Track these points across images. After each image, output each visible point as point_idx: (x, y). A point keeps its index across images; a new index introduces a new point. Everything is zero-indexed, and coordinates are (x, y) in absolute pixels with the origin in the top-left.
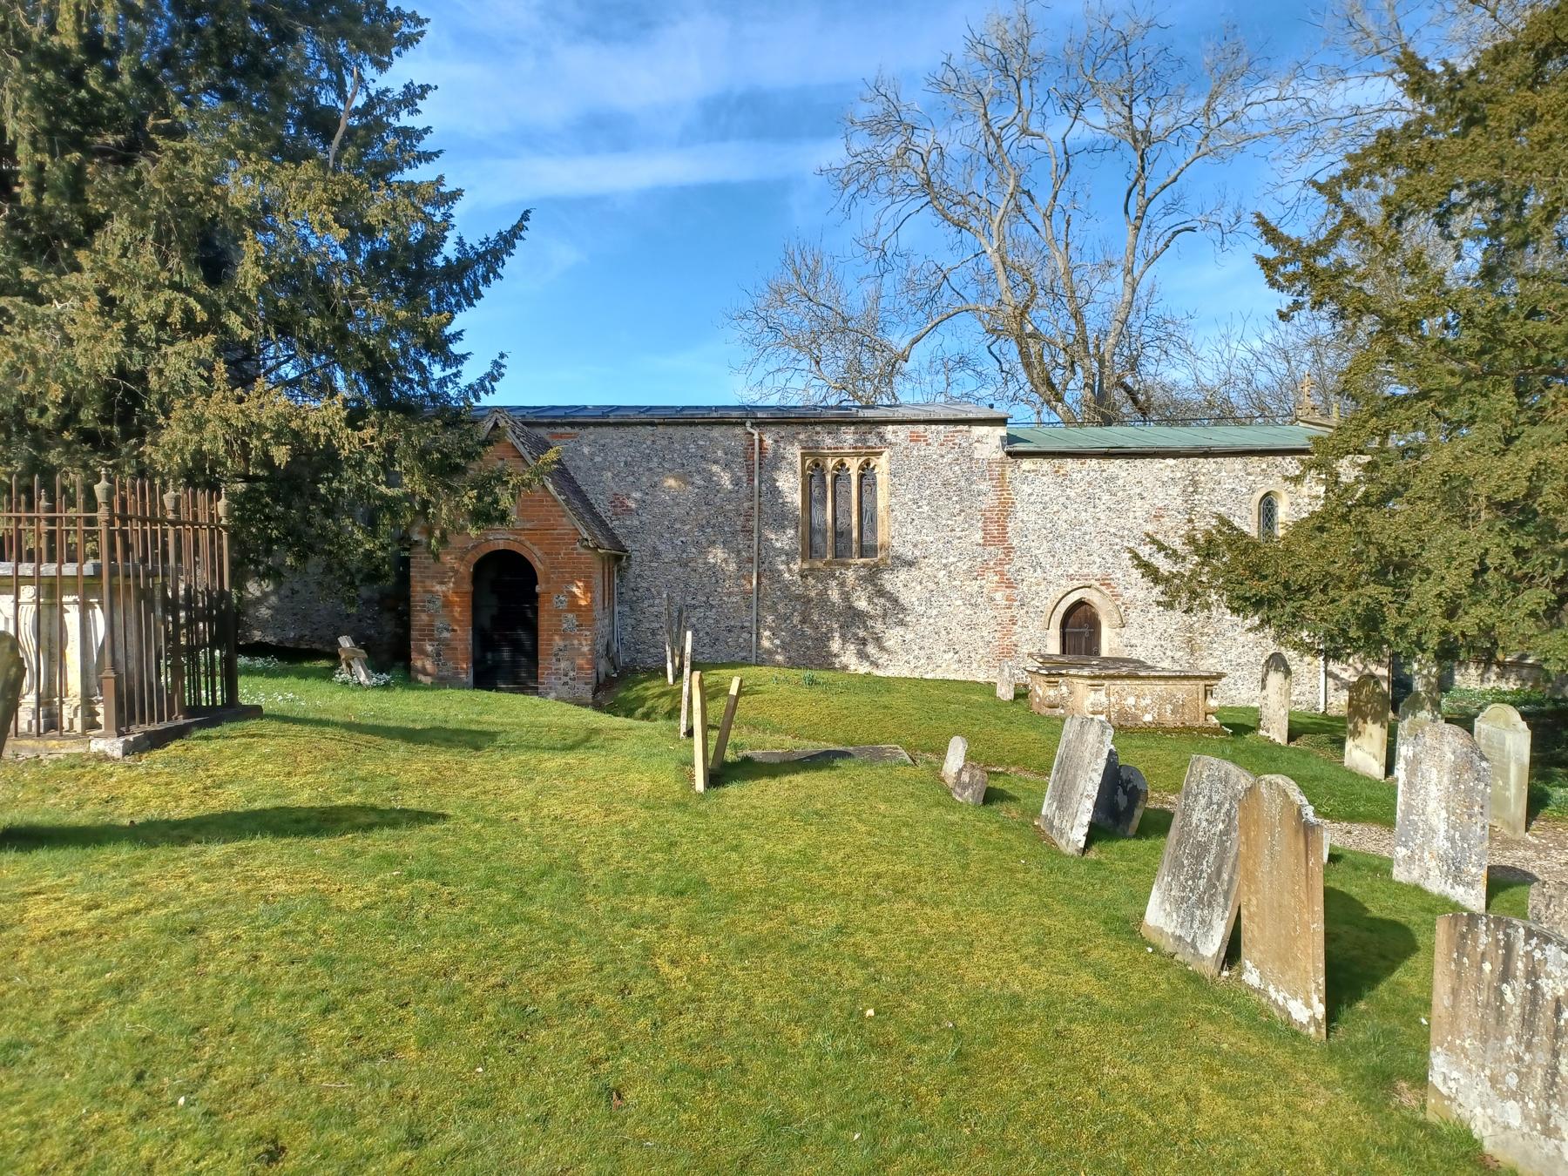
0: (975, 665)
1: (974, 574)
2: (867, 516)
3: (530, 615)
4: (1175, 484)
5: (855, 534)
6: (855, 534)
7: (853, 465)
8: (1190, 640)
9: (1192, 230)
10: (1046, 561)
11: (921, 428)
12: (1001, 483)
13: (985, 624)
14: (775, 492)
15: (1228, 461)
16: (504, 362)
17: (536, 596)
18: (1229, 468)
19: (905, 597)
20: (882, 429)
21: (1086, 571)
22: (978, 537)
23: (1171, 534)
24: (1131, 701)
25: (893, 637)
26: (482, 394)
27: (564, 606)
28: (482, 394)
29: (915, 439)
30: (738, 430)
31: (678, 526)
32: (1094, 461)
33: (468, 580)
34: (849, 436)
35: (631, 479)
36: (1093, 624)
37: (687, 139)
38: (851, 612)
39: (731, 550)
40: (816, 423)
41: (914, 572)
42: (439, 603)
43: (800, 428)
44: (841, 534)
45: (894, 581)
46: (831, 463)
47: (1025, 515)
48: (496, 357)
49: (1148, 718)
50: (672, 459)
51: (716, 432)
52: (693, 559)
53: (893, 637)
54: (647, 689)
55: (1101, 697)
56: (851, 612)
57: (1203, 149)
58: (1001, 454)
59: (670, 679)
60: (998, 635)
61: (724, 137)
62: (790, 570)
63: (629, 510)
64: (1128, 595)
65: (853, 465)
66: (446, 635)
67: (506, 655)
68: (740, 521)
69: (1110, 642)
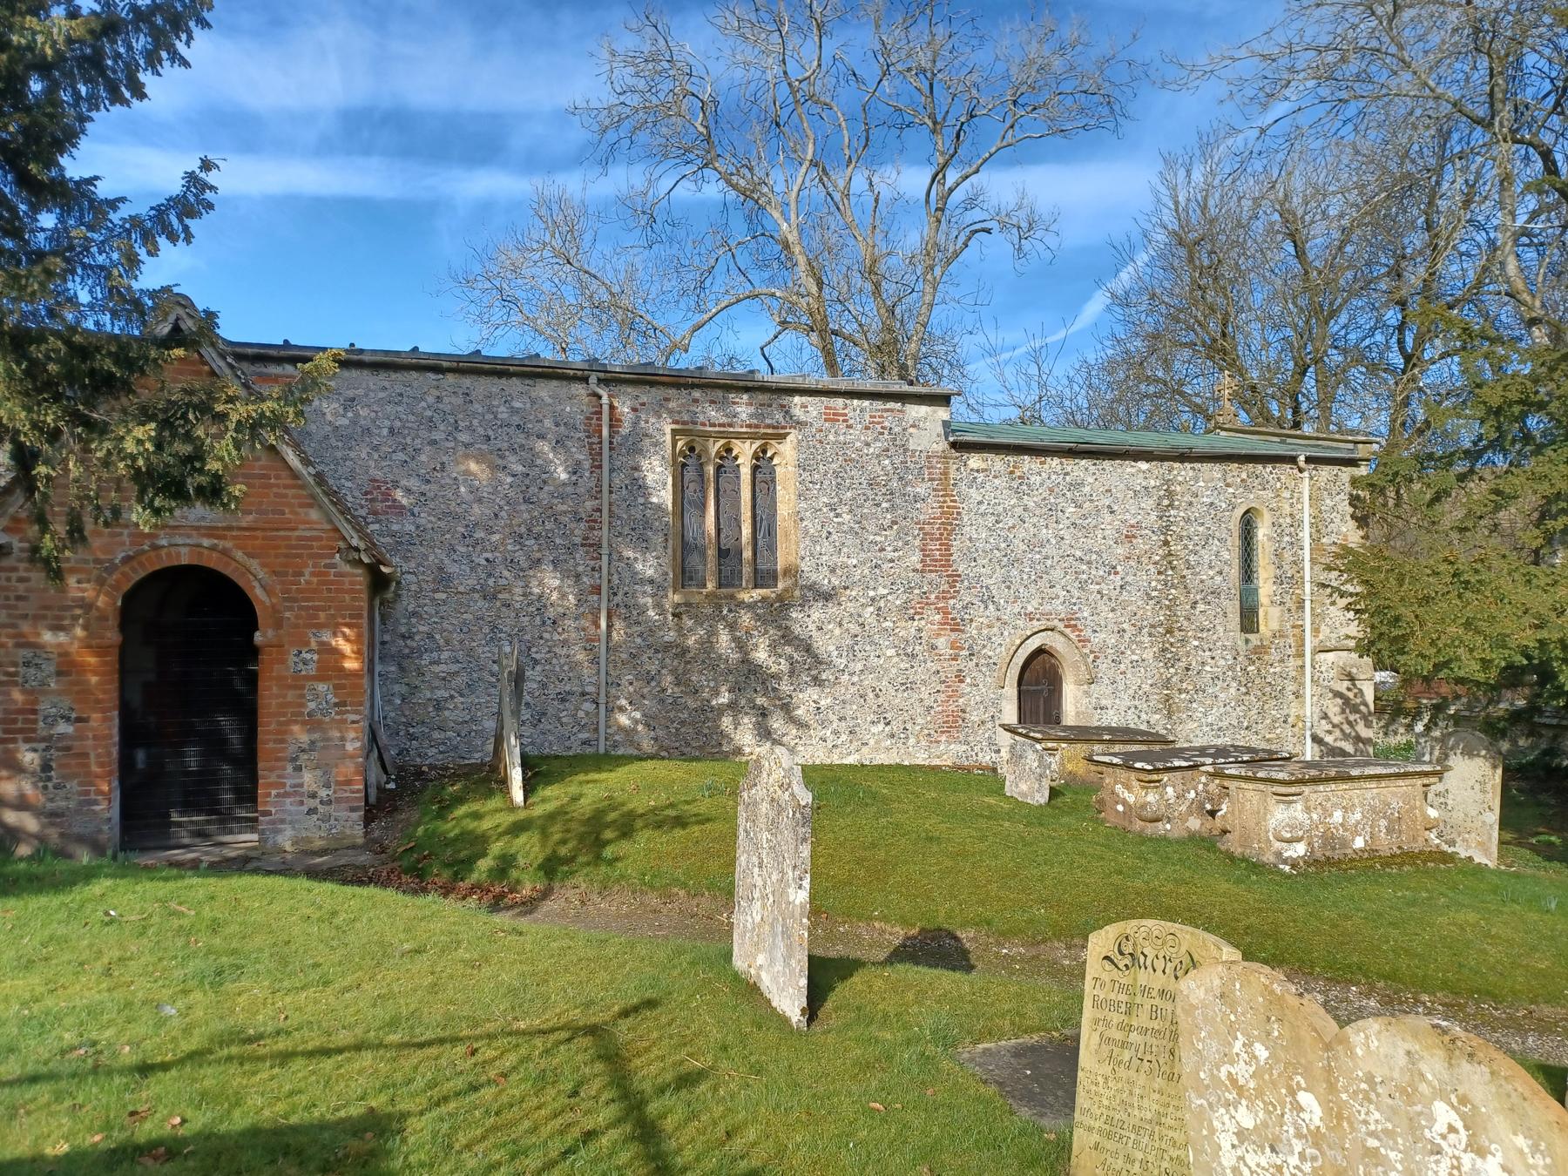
0: (912, 741)
1: (909, 613)
2: (764, 524)
3: (239, 685)
4: (1148, 494)
5: (747, 554)
6: (747, 554)
7: (745, 452)
8: (1168, 698)
9: (988, 231)
10: (1001, 595)
11: (840, 402)
12: (944, 485)
13: (924, 682)
14: (638, 487)
15: (1206, 467)
16: (211, 178)
17: (253, 652)
18: (1207, 476)
19: (825, 645)
20: (786, 400)
21: (1047, 608)
22: (915, 559)
23: (1144, 560)
24: (1338, 816)
25: (806, 700)
26: (162, 241)
27: (312, 669)
28: (162, 241)
29: (833, 417)
30: (579, 389)
31: (480, 534)
32: (1056, 461)
33: (113, 622)
34: (743, 408)
35: (401, 456)
36: (1052, 681)
37: (323, 149)
38: (745, 668)
39: (565, 575)
40: (694, 386)
41: (832, 609)
42: (50, 668)
43: (672, 392)
44: (728, 555)
45: (809, 621)
46: (715, 447)
47: (974, 530)
48: (194, 165)
49: (1359, 843)
50: (470, 428)
51: (544, 391)
52: (505, 589)
53: (806, 700)
54: (477, 816)
55: (1297, 811)
56: (745, 668)
57: (1009, 138)
58: (943, 445)
59: (518, 795)
60: (942, 697)
61: (367, 151)
62: (658, 605)
63: (399, 509)
64: (1097, 640)
65: (745, 452)
66: (63, 728)
67: (192, 760)
68: (579, 530)
69: (1074, 704)
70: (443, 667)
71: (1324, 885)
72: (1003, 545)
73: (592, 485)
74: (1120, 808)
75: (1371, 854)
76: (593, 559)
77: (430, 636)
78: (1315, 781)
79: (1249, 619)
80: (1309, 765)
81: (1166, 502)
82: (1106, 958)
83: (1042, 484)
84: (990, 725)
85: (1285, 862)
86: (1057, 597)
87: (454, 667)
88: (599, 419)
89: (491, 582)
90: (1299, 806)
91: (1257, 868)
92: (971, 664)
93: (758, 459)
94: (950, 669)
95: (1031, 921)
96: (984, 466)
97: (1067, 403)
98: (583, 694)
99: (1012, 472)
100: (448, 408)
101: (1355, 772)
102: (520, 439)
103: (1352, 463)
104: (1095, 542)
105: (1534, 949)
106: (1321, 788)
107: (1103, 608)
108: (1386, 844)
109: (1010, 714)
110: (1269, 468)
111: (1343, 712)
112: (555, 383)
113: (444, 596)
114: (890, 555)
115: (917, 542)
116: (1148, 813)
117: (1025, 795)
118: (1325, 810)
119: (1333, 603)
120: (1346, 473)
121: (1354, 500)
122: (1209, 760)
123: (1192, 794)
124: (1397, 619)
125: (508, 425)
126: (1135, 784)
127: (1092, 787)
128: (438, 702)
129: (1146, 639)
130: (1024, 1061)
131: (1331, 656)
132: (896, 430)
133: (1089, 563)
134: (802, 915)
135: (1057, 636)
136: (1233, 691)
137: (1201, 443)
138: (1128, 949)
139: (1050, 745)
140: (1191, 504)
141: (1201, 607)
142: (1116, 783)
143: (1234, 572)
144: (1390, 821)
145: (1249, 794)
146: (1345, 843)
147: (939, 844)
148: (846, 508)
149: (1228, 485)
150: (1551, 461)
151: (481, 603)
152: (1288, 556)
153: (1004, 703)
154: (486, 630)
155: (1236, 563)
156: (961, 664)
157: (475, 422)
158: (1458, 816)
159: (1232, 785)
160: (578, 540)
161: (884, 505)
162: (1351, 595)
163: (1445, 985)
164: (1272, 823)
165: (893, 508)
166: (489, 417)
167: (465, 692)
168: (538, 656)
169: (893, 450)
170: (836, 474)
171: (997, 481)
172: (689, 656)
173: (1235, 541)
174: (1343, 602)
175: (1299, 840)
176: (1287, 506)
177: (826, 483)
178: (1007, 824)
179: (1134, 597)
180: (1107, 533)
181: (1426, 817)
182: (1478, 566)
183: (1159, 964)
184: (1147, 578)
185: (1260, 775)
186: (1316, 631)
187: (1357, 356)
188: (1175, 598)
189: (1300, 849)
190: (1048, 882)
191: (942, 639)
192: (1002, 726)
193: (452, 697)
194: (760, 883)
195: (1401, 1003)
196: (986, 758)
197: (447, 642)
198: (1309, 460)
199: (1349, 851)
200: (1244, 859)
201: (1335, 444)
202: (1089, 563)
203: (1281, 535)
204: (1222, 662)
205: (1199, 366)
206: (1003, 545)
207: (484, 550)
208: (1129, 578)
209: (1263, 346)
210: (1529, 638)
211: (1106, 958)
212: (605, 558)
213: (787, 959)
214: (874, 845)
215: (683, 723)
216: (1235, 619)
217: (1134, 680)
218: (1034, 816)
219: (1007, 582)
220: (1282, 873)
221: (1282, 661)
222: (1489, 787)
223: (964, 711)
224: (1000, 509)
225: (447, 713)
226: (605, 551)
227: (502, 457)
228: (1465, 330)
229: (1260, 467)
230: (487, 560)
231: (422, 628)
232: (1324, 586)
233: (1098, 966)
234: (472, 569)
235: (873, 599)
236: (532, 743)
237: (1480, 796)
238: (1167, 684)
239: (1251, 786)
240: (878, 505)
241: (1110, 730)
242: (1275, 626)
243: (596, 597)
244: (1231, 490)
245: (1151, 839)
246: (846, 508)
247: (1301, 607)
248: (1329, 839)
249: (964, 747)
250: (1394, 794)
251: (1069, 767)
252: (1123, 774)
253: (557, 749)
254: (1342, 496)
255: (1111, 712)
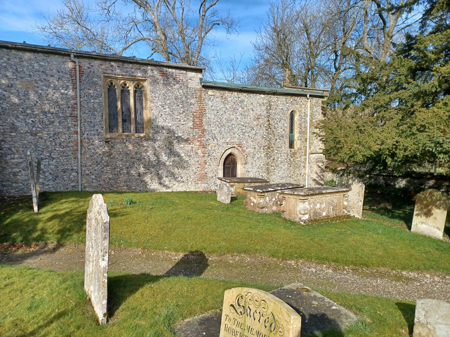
0: (190, 183)
4: (264, 105)
8: (268, 168)
9: (219, 24)
12: (200, 100)
13: (194, 164)
15: (281, 97)
18: (281, 100)
22: (191, 124)
32: (236, 93)
36: (234, 163)
40: (111, 60)
47: (210, 115)
49: (324, 214)
55: (306, 205)
58: (200, 86)
60: (199, 169)
64: (247, 151)
68: (69, 111)
69: (240, 171)
70: (16, 160)
71: (314, 228)
72: (219, 120)
73: (74, 94)
74: (252, 204)
75: (328, 217)
76: (74, 121)
77: (10, 149)
78: (312, 195)
79: (291, 145)
80: (310, 189)
81: (269, 108)
82: (232, 305)
83: (231, 101)
84: (214, 178)
85: (302, 221)
86: (236, 137)
87: (21, 160)
88: (75, 71)
89: (34, 129)
90: (307, 203)
91: (293, 223)
92: (209, 159)
93: (136, 88)
94: (202, 160)
95: (220, 248)
96: (213, 94)
97: (241, 79)
98: (72, 170)
99: (222, 96)
100: (13, 63)
101: (324, 192)
102: (44, 77)
103: (322, 97)
104: (248, 120)
105: (377, 248)
106: (314, 197)
107: (250, 141)
108: (332, 214)
109: (221, 175)
110: (299, 98)
111: (321, 172)
112: (57, 56)
113: (15, 134)
114: (182, 123)
115: (191, 119)
116: (260, 206)
117: (223, 200)
118: (314, 204)
119: (317, 139)
120: (320, 100)
121: (323, 108)
122: (279, 188)
123: (274, 199)
124: (339, 142)
125: (39, 71)
126: (257, 196)
127: (245, 197)
128: (14, 173)
129: (262, 150)
130: (203, 327)
131: (314, 155)
132: (184, 80)
133: (246, 126)
134: (104, 272)
135: (236, 149)
136: (286, 166)
137: (279, 90)
138: (242, 304)
139: (232, 184)
140: (276, 108)
141: (278, 140)
142: (251, 196)
143: (288, 130)
144: (333, 207)
145: (291, 200)
146: (320, 214)
147: (191, 220)
148: (167, 107)
149: (287, 103)
150: (379, 95)
151: (30, 137)
152: (303, 125)
153: (219, 171)
154: (33, 147)
155: (288, 127)
156: (205, 158)
157: (25, 69)
158: (351, 203)
159: (286, 196)
160: (68, 115)
161: (180, 106)
162: (322, 136)
163: (352, 263)
164: (298, 209)
165: (183, 107)
166: (31, 67)
167: (26, 169)
168: (54, 156)
169: (183, 87)
170: (164, 95)
171: (217, 99)
172: (112, 156)
173: (288, 120)
174: (319, 138)
175: (306, 214)
176: (303, 110)
177: (160, 97)
178: (216, 211)
179: (259, 137)
180: (251, 117)
181: (343, 204)
182: (365, 124)
183: (257, 316)
184: (263, 132)
185: (295, 193)
186: (310, 148)
187: (322, 69)
188: (271, 138)
189: (307, 217)
190: (227, 233)
191: (200, 151)
192: (218, 178)
193: (20, 171)
194: (92, 255)
195: (339, 270)
196: (213, 188)
197: (17, 151)
198: (310, 96)
199: (321, 217)
200: (290, 220)
201: (317, 91)
202: (246, 126)
203: (301, 119)
204: (284, 157)
205: (277, 76)
206: (219, 120)
207: (31, 117)
208: (258, 132)
209: (298, 64)
210: (376, 148)
211: (232, 305)
212: (79, 122)
213: (99, 290)
214: (168, 222)
215: (110, 179)
216: (288, 144)
217: (258, 163)
218: (227, 208)
219: (220, 132)
220: (301, 225)
221: (300, 157)
222: (361, 194)
223: (206, 173)
224: (218, 108)
225: (18, 177)
226: (79, 118)
227: (37, 83)
228: (357, 54)
229: (296, 98)
230: (32, 121)
231: (6, 146)
232: (314, 133)
233: (228, 309)
234: (26, 124)
235: (177, 137)
236: (53, 187)
237: (358, 197)
238: (268, 164)
239: (292, 197)
240: (178, 106)
241: (251, 179)
242: (299, 146)
243: (76, 135)
244: (288, 105)
245: (261, 214)
246: (167, 107)
247: (306, 141)
248: (315, 213)
249: (206, 185)
250: (335, 198)
251: (238, 191)
252: (253, 193)
253: (62, 189)
254: (319, 107)
255: (251, 173)
